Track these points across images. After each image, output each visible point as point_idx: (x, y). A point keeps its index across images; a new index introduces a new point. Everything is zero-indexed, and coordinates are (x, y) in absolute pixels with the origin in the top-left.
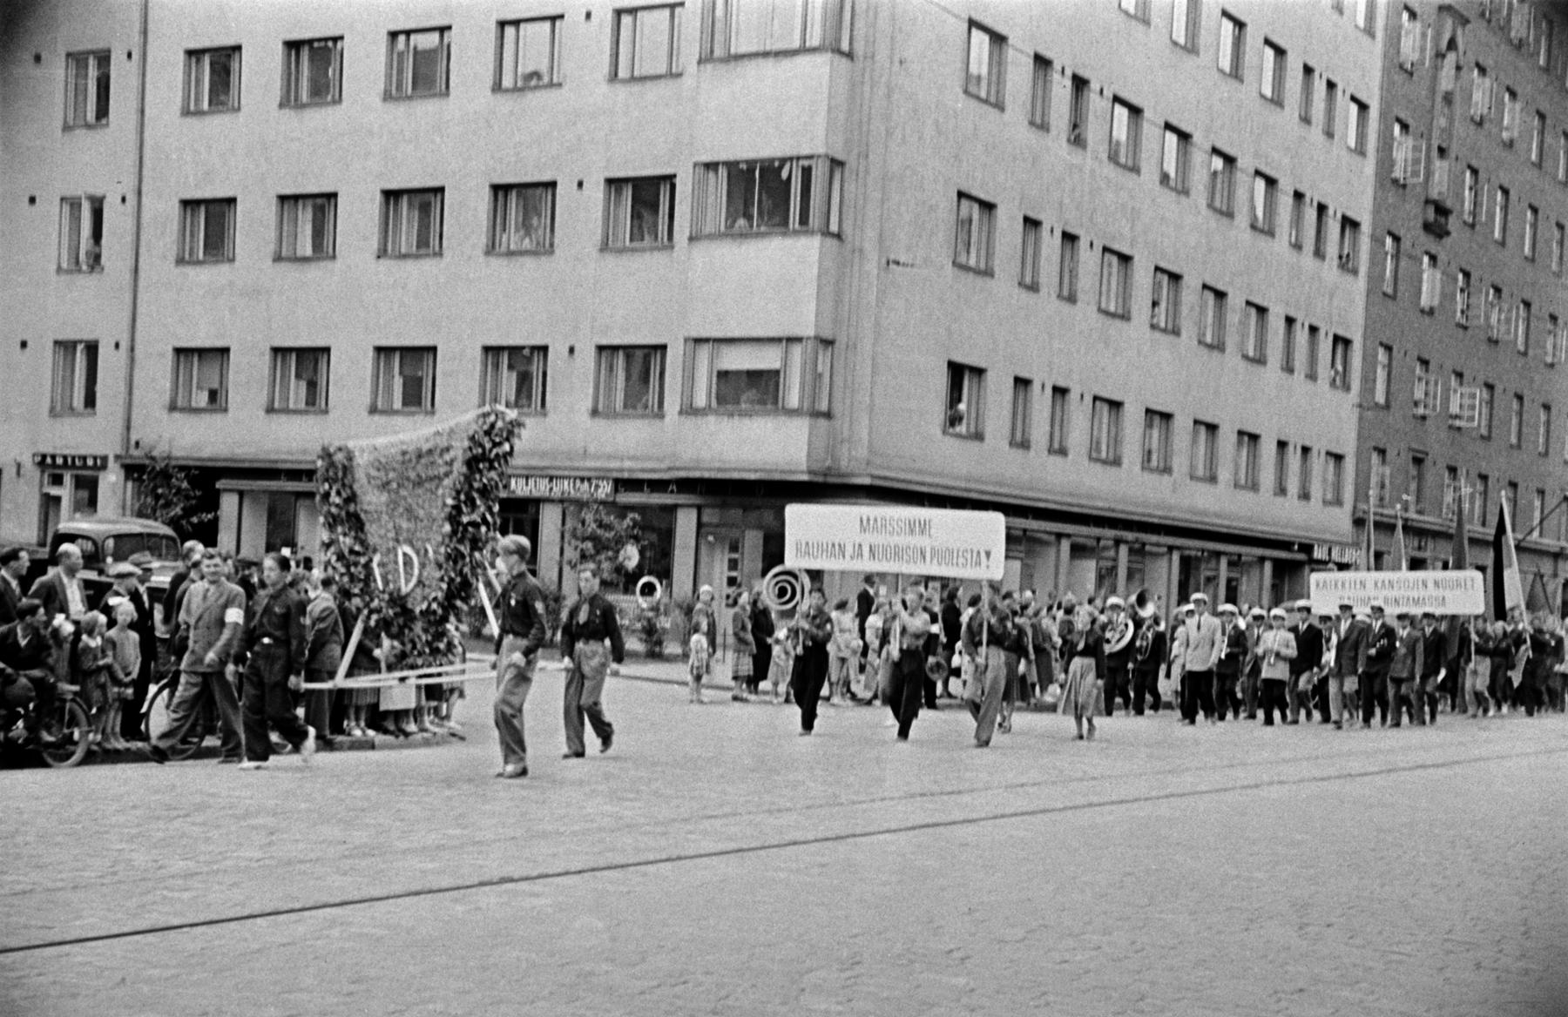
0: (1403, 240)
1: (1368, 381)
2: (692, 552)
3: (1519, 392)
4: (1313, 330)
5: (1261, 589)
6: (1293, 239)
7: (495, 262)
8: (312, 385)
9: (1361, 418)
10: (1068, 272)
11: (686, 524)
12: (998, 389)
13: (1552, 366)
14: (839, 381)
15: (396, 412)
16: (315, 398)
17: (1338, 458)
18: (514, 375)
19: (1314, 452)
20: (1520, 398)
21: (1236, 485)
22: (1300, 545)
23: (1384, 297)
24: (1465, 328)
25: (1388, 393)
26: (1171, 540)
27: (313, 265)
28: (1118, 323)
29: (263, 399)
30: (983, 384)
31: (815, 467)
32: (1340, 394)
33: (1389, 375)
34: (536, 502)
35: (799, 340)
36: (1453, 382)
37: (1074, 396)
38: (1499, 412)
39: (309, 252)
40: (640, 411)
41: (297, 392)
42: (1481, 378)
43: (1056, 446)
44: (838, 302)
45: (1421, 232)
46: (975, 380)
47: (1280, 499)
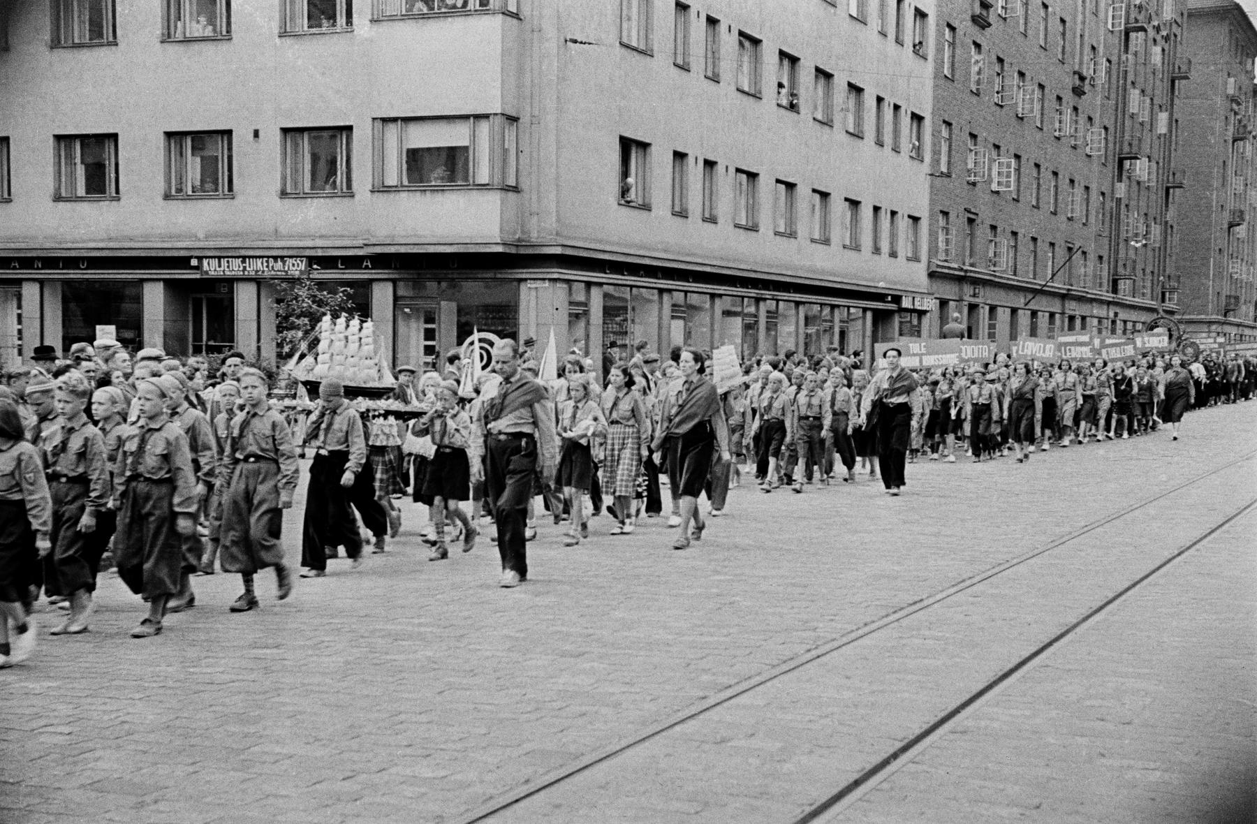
1: (936, 153)
2: (391, 324)
5: (864, 337)
7: (172, 49)
9: (931, 187)
10: (713, 55)
12: (661, 158)
13: (1058, 138)
17: (915, 220)
18: (198, 160)
19: (900, 215)
20: (1037, 166)
21: (844, 247)
22: (893, 296)
25: (949, 163)
26: (798, 297)
30: (648, 159)
31: (510, 238)
33: (950, 146)
34: (230, 282)
35: (486, 116)
36: (994, 153)
37: (720, 168)
38: (1024, 180)
40: (328, 190)
42: (1012, 151)
43: (707, 215)
44: (520, 70)
45: (970, 23)
46: (641, 152)
47: (876, 257)
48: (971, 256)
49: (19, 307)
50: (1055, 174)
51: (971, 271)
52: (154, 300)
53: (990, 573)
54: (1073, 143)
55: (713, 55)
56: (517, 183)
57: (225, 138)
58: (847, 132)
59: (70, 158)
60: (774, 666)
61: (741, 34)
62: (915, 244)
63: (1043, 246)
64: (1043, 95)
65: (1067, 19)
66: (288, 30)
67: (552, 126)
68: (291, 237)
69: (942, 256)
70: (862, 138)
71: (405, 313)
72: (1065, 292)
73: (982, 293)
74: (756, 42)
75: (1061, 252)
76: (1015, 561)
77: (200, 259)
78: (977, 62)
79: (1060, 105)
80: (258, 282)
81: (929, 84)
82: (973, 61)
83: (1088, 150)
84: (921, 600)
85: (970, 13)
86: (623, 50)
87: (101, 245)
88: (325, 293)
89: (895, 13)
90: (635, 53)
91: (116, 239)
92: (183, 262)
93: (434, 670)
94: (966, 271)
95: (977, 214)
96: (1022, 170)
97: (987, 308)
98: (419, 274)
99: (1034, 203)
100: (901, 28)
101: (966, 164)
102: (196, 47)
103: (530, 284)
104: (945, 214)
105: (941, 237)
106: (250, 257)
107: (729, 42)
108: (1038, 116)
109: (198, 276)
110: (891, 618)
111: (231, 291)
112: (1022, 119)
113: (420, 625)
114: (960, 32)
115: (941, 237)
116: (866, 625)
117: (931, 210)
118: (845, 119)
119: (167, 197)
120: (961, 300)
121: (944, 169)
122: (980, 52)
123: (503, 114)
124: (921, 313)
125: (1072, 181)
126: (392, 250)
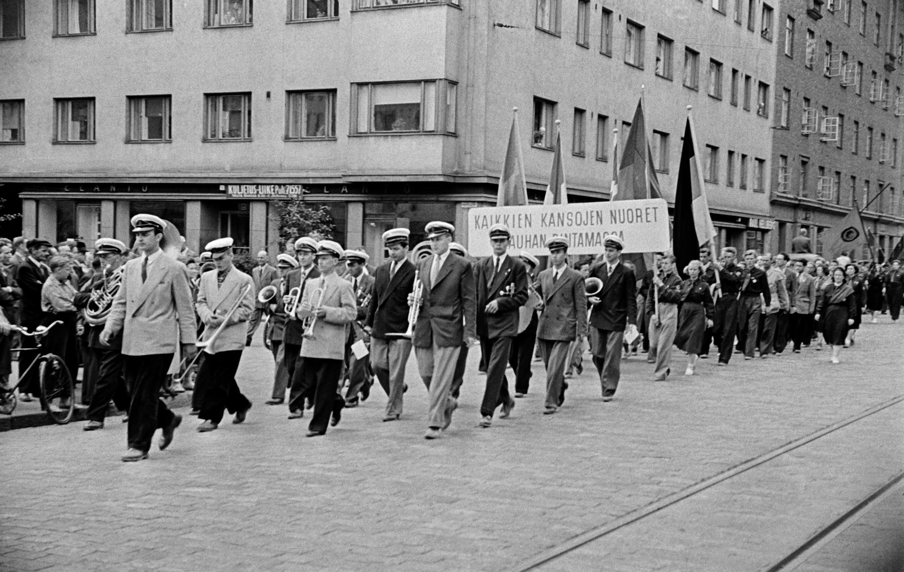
0: (796, 21)
1: (778, 112)
2: (360, 234)
3: (857, 120)
4: (748, 78)
6: (736, 19)
7: (211, 34)
8: (84, 124)
9: (774, 137)
10: (607, 37)
11: (355, 214)
12: (565, 114)
13: (873, 103)
14: (462, 113)
15: (144, 142)
16: (86, 136)
17: (761, 161)
18: (227, 114)
19: (748, 158)
20: (856, 123)
22: (742, 218)
23: (786, 58)
24: (829, 78)
25: (788, 120)
27: (81, 39)
28: (637, 72)
29: (50, 135)
31: (448, 172)
32: (761, 120)
33: (789, 107)
34: (248, 202)
37: (610, 121)
38: (846, 133)
39: (77, 31)
41: (73, 129)
42: (837, 112)
44: (459, 51)
46: (549, 109)
48: (804, 189)
49: (99, 220)
50: (870, 129)
51: (804, 201)
52: (194, 214)
53: (812, 437)
54: (884, 106)
55: (607, 37)
56: (456, 129)
57: (247, 98)
58: (709, 96)
59: (138, 111)
60: (619, 517)
61: (629, 22)
62: (761, 180)
63: (860, 183)
64: (862, 70)
65: (881, 13)
66: (293, 19)
67: (483, 88)
68: (292, 170)
69: (781, 189)
70: (721, 100)
71: (372, 227)
72: (876, 217)
73: (812, 217)
74: (640, 28)
75: (874, 187)
76: (835, 426)
77: (226, 185)
78: (811, 45)
79: (875, 78)
80: (267, 202)
81: (773, 60)
82: (808, 44)
83: (896, 113)
84: (753, 459)
85: (806, 8)
86: (538, 33)
87: (159, 175)
88: (310, 209)
89: (747, 6)
90: (547, 36)
91: (168, 171)
92: (214, 188)
93: (328, 511)
94: (800, 200)
95: (809, 158)
96: (845, 126)
97: (816, 229)
98: (382, 198)
99: (854, 151)
100: (752, 15)
101: (801, 121)
102: (228, 31)
103: (463, 206)
104: (784, 157)
105: (781, 175)
106: (261, 184)
107: (619, 28)
108: (858, 86)
109: (225, 198)
110: (726, 475)
111: (248, 210)
112: (845, 88)
113: (329, 470)
114: (798, 22)
115: (781, 175)
116: (703, 480)
117: (773, 154)
118: (707, 87)
119: (205, 140)
120: (795, 222)
121: (784, 124)
122: (813, 37)
123: (446, 79)
124: (764, 232)
125: (883, 135)
126: (363, 179)
